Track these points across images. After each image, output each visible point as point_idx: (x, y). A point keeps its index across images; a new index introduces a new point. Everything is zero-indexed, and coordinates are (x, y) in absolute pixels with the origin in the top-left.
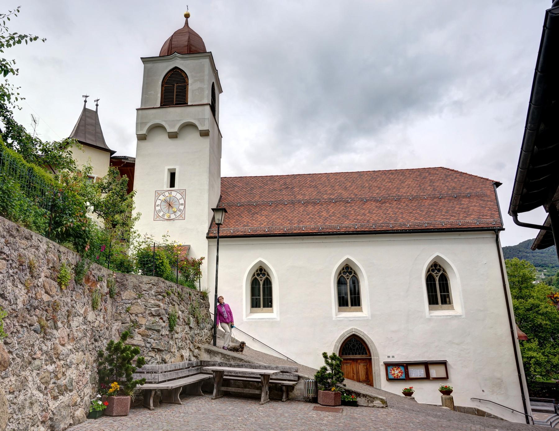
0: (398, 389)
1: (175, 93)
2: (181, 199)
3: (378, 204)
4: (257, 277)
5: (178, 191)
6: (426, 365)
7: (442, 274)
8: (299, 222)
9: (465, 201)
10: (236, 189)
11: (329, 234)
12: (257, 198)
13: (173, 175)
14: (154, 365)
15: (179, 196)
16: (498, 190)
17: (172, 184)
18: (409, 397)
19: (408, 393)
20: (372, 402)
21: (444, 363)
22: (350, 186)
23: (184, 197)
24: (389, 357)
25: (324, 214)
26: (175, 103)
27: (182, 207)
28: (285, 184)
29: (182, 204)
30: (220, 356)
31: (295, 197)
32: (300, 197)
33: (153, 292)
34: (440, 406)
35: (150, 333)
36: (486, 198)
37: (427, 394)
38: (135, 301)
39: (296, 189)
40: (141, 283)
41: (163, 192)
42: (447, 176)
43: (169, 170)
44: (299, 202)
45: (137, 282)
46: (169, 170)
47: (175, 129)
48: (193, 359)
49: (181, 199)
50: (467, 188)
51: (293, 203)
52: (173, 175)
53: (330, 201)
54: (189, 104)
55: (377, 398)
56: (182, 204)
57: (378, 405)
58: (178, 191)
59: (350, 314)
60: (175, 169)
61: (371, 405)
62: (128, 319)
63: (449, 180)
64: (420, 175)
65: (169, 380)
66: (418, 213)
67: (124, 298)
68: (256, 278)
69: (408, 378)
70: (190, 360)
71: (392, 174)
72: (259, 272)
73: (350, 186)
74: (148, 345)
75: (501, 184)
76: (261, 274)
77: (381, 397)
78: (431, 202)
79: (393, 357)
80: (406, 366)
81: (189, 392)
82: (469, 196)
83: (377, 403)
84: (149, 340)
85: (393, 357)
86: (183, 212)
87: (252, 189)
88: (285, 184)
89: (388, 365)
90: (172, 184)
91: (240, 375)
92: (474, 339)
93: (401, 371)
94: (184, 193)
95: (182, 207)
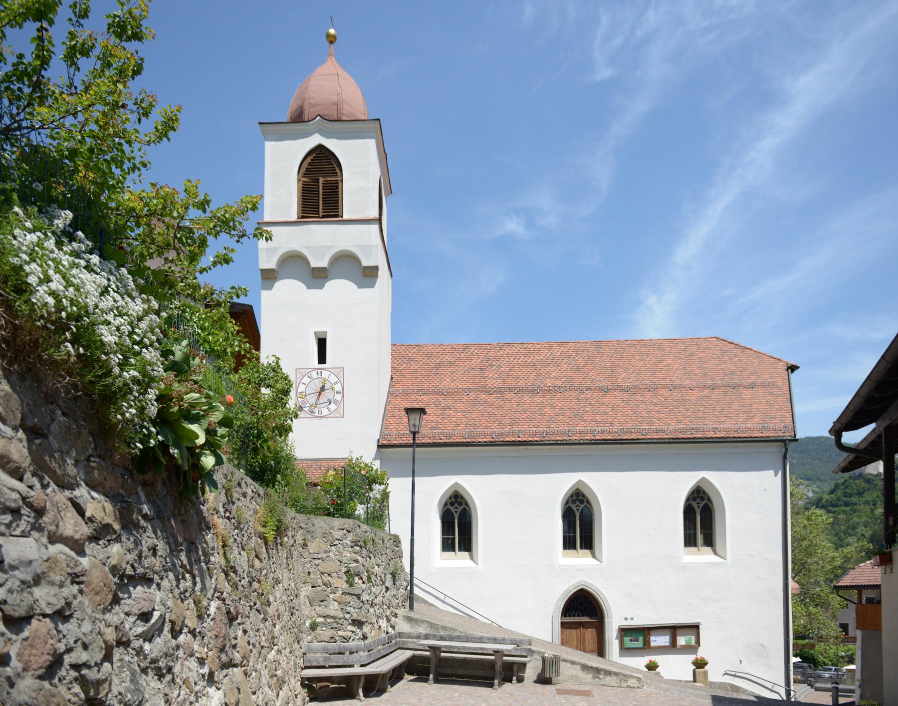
0: (639, 662)
1: (321, 196)
2: (336, 383)
3: (625, 396)
4: (451, 508)
5: (332, 370)
6: (673, 630)
7: (706, 504)
8: (512, 424)
9: (747, 394)
10: (414, 366)
11: (557, 443)
12: (446, 382)
13: (322, 344)
14: (355, 643)
15: (333, 379)
16: (794, 376)
17: (322, 359)
18: (653, 672)
19: (652, 667)
20: (626, 681)
21: (694, 628)
22: (584, 366)
23: (341, 380)
24: (626, 619)
25: (548, 410)
26: (321, 214)
27: (338, 397)
28: (487, 358)
29: (338, 392)
30: (426, 625)
31: (504, 381)
32: (511, 382)
33: (348, 541)
34: (690, 682)
35: (348, 598)
36: (775, 390)
37: (676, 667)
38: (326, 555)
39: (505, 369)
40: (332, 528)
41: (308, 371)
42: (723, 352)
43: (316, 333)
44: (510, 390)
45: (327, 528)
46: (316, 333)
47: (324, 263)
48: (390, 630)
49: (336, 383)
50: (751, 374)
51: (501, 391)
52: (322, 344)
53: (557, 389)
54: (345, 217)
55: (632, 676)
56: (338, 392)
57: (632, 685)
58: (332, 370)
59: (580, 559)
60: (326, 333)
61: (624, 685)
62: (319, 581)
63: (726, 358)
64: (685, 350)
65: (373, 662)
66: (680, 412)
67: (311, 551)
68: (448, 509)
69: (647, 647)
70: (387, 633)
71: (645, 346)
72: (453, 500)
73: (584, 366)
74: (347, 616)
75: (798, 368)
76: (456, 502)
77: (636, 675)
78: (701, 394)
79: (632, 619)
80: (646, 632)
81: (395, 676)
82: (752, 386)
83: (632, 682)
84: (348, 609)
85: (632, 619)
86: (341, 405)
87: (438, 366)
88: (487, 358)
89: (624, 632)
90: (322, 359)
91: (455, 650)
92: (734, 595)
93: (638, 636)
94: (341, 373)
95: (338, 397)
